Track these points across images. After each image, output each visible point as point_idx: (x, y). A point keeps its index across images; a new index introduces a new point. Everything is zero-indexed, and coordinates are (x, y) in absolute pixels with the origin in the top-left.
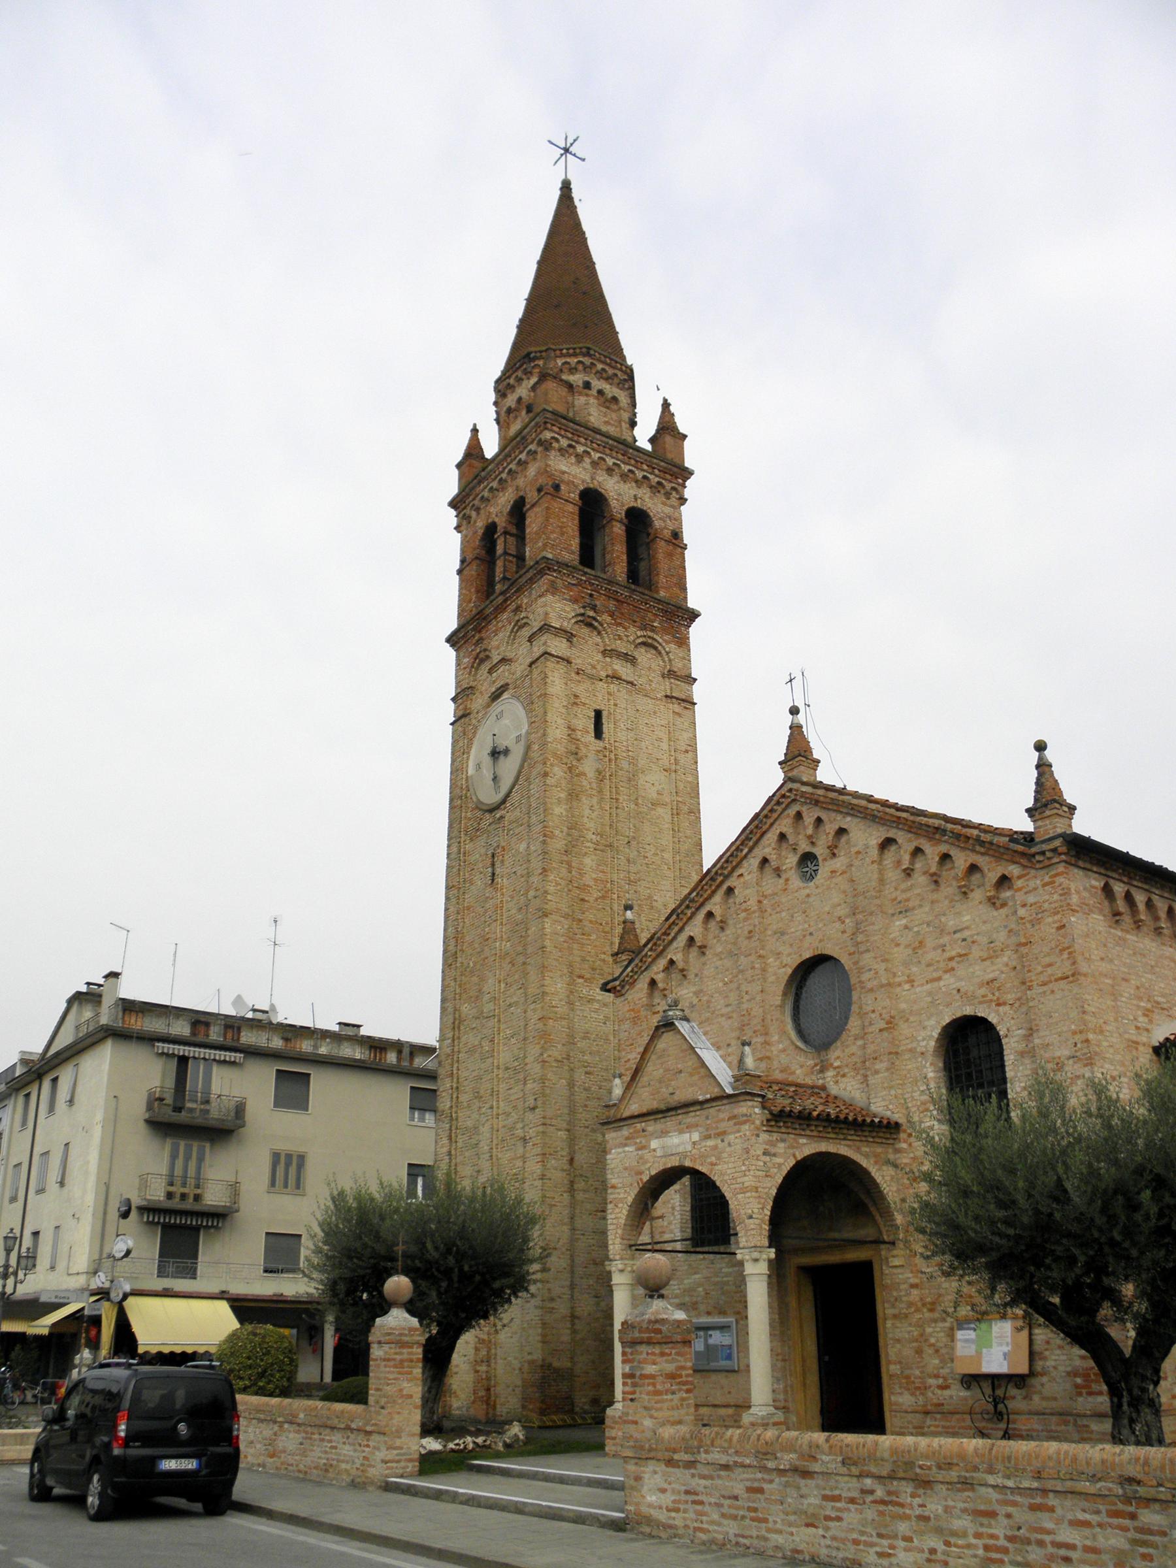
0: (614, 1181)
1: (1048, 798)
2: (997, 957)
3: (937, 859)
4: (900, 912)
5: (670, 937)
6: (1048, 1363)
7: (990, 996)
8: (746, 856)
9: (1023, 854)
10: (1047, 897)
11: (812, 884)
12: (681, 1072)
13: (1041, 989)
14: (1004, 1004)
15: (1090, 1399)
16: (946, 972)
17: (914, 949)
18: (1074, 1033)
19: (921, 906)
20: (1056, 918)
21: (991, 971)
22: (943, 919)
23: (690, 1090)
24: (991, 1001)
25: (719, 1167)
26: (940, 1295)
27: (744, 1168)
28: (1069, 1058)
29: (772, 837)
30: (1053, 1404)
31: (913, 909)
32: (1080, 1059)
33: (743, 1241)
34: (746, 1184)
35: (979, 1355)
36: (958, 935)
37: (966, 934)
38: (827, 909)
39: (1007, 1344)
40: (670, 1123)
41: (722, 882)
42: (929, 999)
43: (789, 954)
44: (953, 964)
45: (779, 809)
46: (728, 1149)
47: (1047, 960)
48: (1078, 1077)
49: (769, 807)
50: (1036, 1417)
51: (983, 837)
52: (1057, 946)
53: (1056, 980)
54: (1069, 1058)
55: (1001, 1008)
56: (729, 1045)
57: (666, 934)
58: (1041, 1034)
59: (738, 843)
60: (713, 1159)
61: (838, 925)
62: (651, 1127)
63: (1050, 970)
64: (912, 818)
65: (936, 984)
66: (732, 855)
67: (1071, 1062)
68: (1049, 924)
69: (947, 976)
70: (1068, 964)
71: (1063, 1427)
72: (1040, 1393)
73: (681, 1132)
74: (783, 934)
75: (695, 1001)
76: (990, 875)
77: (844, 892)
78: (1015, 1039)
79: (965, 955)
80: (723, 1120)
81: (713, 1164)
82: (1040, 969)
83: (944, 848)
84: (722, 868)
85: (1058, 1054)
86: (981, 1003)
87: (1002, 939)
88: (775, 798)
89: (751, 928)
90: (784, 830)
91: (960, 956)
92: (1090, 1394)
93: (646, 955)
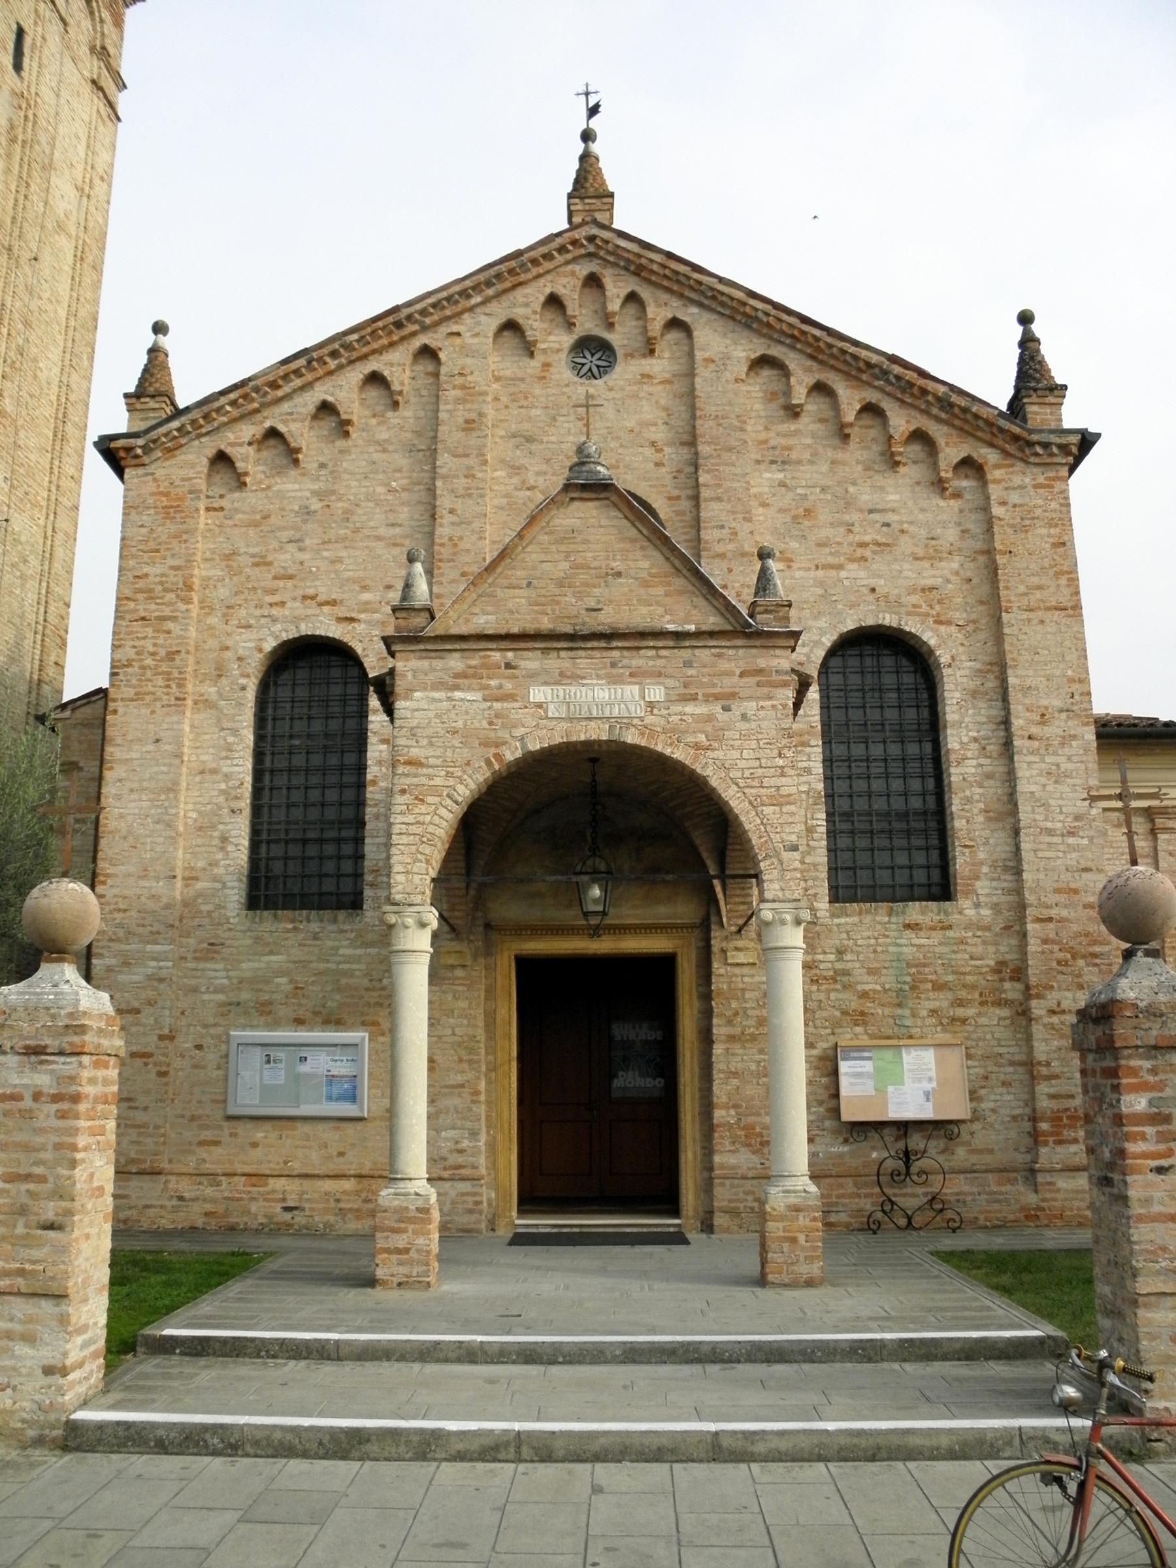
0: (415, 752)
1: (1032, 373)
2: (941, 559)
3: (858, 407)
4: (773, 462)
5: (280, 393)
6: (983, 1105)
7: (925, 608)
8: (471, 309)
9: (1016, 438)
10: (1040, 502)
11: (599, 382)
12: (619, 574)
13: (1025, 615)
14: (949, 623)
15: (1059, 1149)
16: (852, 560)
17: (795, 517)
18: (1071, 680)
19: (811, 462)
20: (1052, 531)
21: (930, 576)
22: (851, 489)
23: (644, 610)
24: (927, 615)
25: (718, 754)
26: (845, 1013)
27: (781, 762)
28: (1061, 711)
29: (536, 293)
30: (987, 1159)
31: (799, 462)
32: (1079, 716)
33: (772, 889)
34: (784, 791)
35: (881, 1091)
36: (875, 516)
37: (891, 517)
38: (630, 424)
39: (930, 1079)
40: (584, 661)
41: (414, 334)
42: (820, 591)
43: (539, 473)
44: (867, 553)
45: (560, 259)
46: (743, 726)
47: (1035, 580)
48: (1074, 737)
49: (544, 250)
50: (962, 1176)
51: (954, 398)
52: (1051, 567)
53: (1048, 609)
54: (1061, 711)
55: (942, 628)
56: (389, 587)
57: (274, 385)
58: (1020, 672)
59: (468, 283)
60: (702, 738)
61: (648, 452)
62: (531, 661)
63: (1038, 594)
64: (829, 340)
65: (833, 573)
66: (448, 299)
67: (1064, 715)
68: (1042, 537)
69: (853, 566)
70: (1066, 592)
71: (1008, 1188)
72: (969, 1144)
73: (615, 680)
74: (530, 440)
75: (315, 505)
76: (948, 450)
77: (666, 409)
78: (963, 672)
79: (888, 545)
80: (730, 674)
81: (697, 746)
82: (1022, 589)
83: (873, 396)
84: (424, 312)
85: (1044, 702)
86: (909, 614)
87: (951, 539)
88: (559, 240)
89: (473, 416)
90: (561, 291)
91: (879, 545)
92: (1060, 1142)
93: (218, 410)
